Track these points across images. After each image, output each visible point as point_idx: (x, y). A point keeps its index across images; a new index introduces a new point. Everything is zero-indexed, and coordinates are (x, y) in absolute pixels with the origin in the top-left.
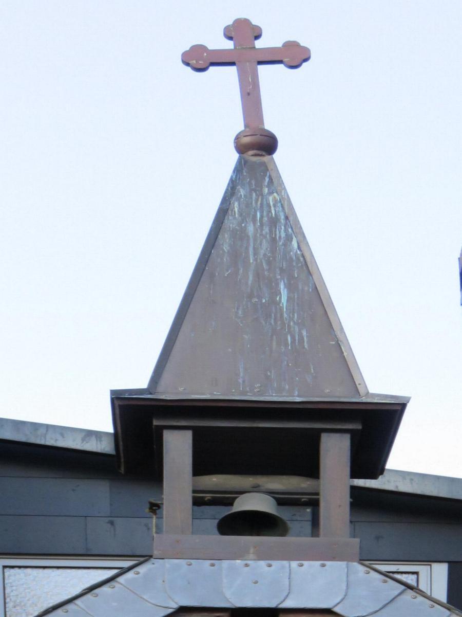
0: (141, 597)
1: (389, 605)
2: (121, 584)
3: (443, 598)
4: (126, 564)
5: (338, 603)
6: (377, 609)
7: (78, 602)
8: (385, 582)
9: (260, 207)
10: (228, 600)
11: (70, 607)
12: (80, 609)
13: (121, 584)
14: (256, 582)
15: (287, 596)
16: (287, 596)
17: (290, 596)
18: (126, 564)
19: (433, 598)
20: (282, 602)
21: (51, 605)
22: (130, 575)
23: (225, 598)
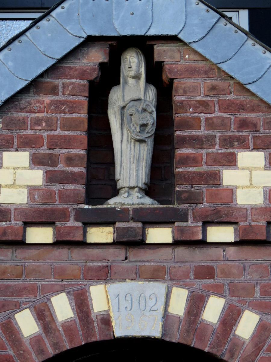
0: (65, 29)
1: (211, 31)
2: (53, 17)
3: (246, 28)
4: (37, 15)
5: (181, 31)
6: (204, 35)
7: (28, 34)
8: (208, 11)
9: (120, 173)
10: (115, 29)
11: (23, 38)
12: (29, 40)
13: (53, 17)
14: (132, 14)
15: (151, 25)
16: (151, 25)
17: (153, 25)
18: (37, 15)
19: (240, 27)
20: (147, 32)
21: (10, 37)
22: (44, 22)
23: (114, 27)
